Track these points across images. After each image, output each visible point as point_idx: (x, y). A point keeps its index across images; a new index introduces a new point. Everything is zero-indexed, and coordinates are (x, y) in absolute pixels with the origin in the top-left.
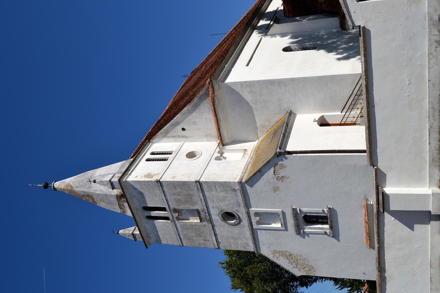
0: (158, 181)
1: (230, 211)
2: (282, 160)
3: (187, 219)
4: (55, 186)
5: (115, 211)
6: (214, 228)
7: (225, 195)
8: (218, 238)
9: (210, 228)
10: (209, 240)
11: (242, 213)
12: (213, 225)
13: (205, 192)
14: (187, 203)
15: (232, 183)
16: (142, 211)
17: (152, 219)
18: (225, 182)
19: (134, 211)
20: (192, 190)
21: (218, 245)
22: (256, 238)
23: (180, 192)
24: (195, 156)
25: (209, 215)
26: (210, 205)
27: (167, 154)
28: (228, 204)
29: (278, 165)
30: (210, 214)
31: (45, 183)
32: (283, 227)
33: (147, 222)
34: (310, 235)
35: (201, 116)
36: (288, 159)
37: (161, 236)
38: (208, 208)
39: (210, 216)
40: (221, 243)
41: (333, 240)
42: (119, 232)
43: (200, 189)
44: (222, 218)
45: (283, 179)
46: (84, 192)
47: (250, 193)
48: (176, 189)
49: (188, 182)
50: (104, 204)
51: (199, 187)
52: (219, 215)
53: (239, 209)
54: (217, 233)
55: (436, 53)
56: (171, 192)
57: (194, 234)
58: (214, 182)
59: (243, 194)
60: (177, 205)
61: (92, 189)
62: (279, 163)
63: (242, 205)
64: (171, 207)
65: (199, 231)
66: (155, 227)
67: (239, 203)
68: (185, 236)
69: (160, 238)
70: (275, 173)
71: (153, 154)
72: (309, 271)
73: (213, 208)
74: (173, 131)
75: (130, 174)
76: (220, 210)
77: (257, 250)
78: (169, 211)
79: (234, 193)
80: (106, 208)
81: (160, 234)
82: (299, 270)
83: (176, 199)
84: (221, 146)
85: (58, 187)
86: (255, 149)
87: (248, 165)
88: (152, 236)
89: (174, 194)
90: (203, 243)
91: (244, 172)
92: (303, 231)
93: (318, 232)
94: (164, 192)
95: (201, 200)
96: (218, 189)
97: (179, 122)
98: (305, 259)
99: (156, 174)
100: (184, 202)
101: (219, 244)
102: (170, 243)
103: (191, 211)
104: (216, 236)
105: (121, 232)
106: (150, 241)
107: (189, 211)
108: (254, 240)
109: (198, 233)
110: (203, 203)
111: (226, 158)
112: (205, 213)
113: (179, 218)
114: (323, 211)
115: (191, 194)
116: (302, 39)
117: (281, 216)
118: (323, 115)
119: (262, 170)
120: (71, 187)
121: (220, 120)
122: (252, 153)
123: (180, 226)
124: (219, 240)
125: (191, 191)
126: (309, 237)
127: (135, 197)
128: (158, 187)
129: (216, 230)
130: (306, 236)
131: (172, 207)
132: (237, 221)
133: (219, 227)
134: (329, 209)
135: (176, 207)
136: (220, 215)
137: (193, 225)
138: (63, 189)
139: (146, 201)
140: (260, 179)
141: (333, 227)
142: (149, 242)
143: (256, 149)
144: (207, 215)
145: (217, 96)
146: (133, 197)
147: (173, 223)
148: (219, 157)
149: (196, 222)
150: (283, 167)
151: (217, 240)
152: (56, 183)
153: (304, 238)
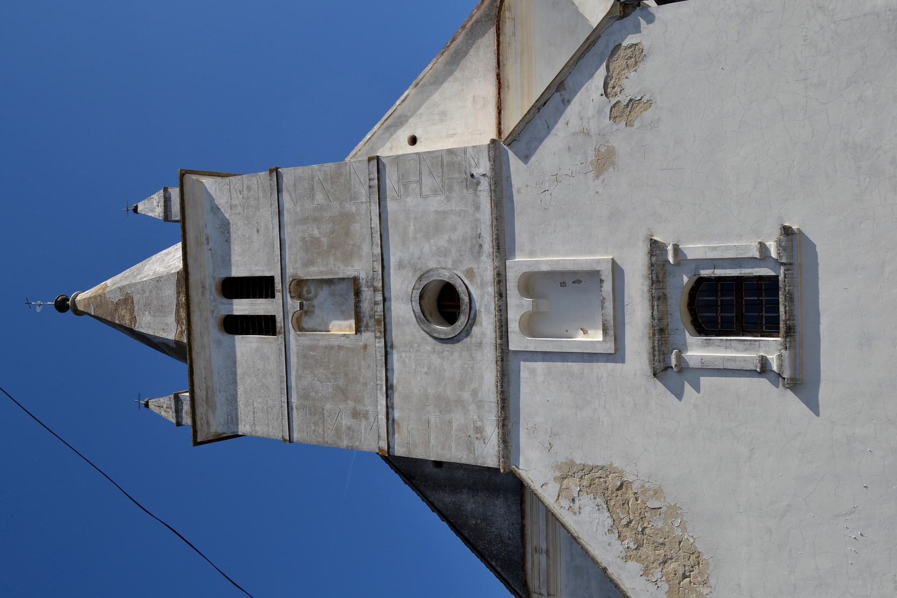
2: (637, 29)
9: (378, 356)
11: (483, 285)
12: (389, 345)
21: (390, 439)
22: (512, 401)
25: (384, 300)
29: (621, 52)
30: (386, 295)
32: (608, 338)
34: (705, 381)
35: (463, 90)
36: (656, 21)
41: (793, 403)
45: (630, 112)
47: (519, 191)
53: (474, 266)
62: (625, 44)
63: (488, 246)
68: (305, 396)
70: (609, 90)
72: (684, 576)
74: (386, 146)
77: (507, 458)
82: (646, 572)
92: (679, 358)
93: (734, 359)
95: (372, 234)
97: (405, 116)
98: (674, 511)
106: (211, 420)
108: (503, 408)
114: (763, 247)
117: (607, 286)
119: (569, 83)
121: (506, 58)
126: (698, 391)
130: (688, 387)
134: (787, 231)
140: (556, 122)
141: (798, 329)
144: (379, 298)
145: (512, 9)
150: (637, 55)
151: (390, 410)
153: (679, 394)
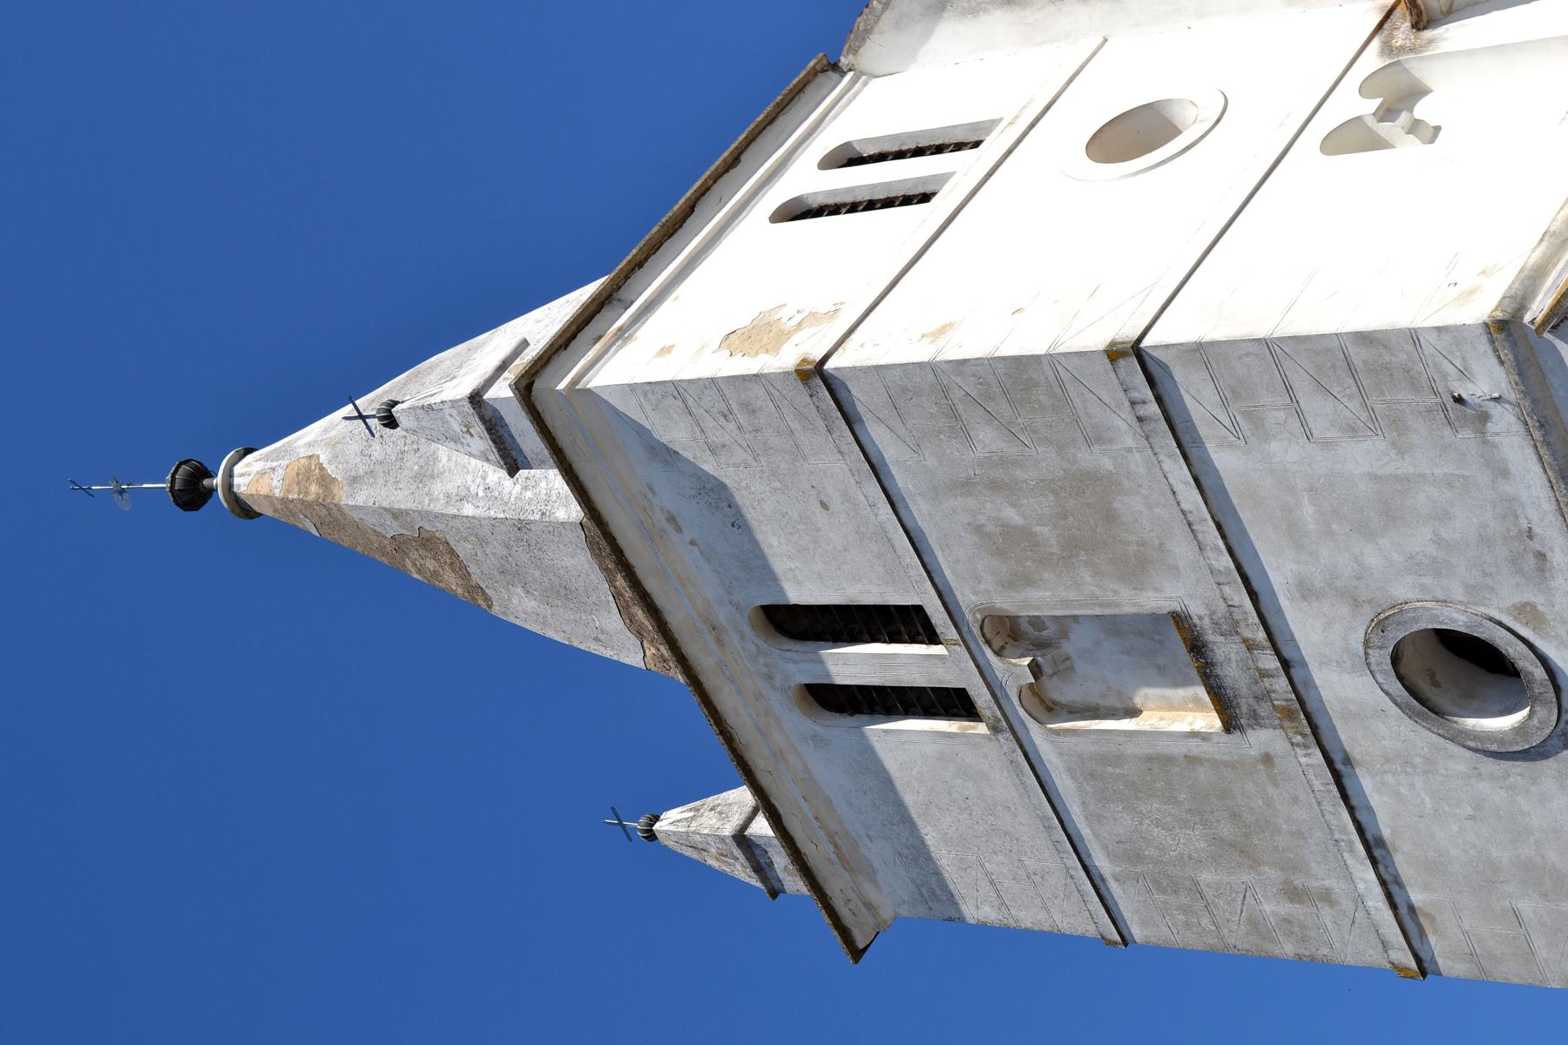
0: (815, 374)
1: (1457, 620)
3: (1118, 705)
4: (239, 486)
5: (608, 653)
6: (1347, 782)
7: (1388, 470)
8: (1404, 878)
10: (1327, 897)
13: (1210, 446)
14: (1083, 556)
15: (1432, 338)
16: (759, 650)
17: (852, 715)
18: (1365, 339)
19: (691, 649)
20: (1099, 440)
21: (1416, 943)
23: (1003, 461)
24: (1172, 131)
25: (1286, 665)
26: (1279, 572)
27: (939, 149)
28: (1432, 550)
30: (1288, 653)
31: (181, 463)
33: (814, 737)
37: (944, 858)
38: (1263, 598)
39: (1293, 671)
40: (1432, 919)
42: (657, 827)
43: (1164, 426)
44: (1397, 688)
46: (396, 514)
48: (965, 435)
49: (1051, 360)
50: (533, 603)
51: (1144, 402)
52: (1372, 660)
53: (1538, 600)
54: (1386, 833)
56: (931, 462)
57: (1194, 841)
58: (1265, 342)
59: (1547, 444)
60: (1012, 583)
61: (438, 488)
64: (960, 598)
65: (1234, 816)
66: (887, 782)
67: (1530, 534)
68: (1131, 854)
69: (937, 873)
71: (849, 157)
73: (1304, 597)
75: (623, 334)
76: (1368, 613)
78: (956, 636)
79: (1466, 434)
80: (551, 634)
81: (931, 837)
83: (990, 528)
84: (1402, 31)
85: (254, 492)
88: (876, 852)
89: (966, 486)
90: (1287, 921)
94: (877, 470)
95: (1190, 525)
96: (1317, 408)
99: (814, 318)
100: (1055, 550)
101: (1422, 933)
102: (1028, 917)
103: (1141, 634)
104: (1377, 853)
105: (671, 822)
107: (1113, 626)
109: (1226, 830)
110: (1210, 553)
111: (1437, 129)
112: (1250, 646)
113: (1054, 703)
115: (1092, 478)
120: (326, 481)
123: (1069, 770)
124: (1417, 897)
125: (1096, 448)
127: (679, 530)
128: (820, 423)
129: (1375, 800)
131: (966, 598)
132: (1541, 712)
133: (1389, 778)
135: (1006, 603)
136: (1382, 658)
137: (1168, 760)
138: (285, 501)
139: (761, 556)
142: (868, 905)
144: (1270, 662)
146: (667, 526)
147: (1006, 739)
148: (1372, 123)
149: (1194, 734)
151: (1394, 888)
152: (249, 458)
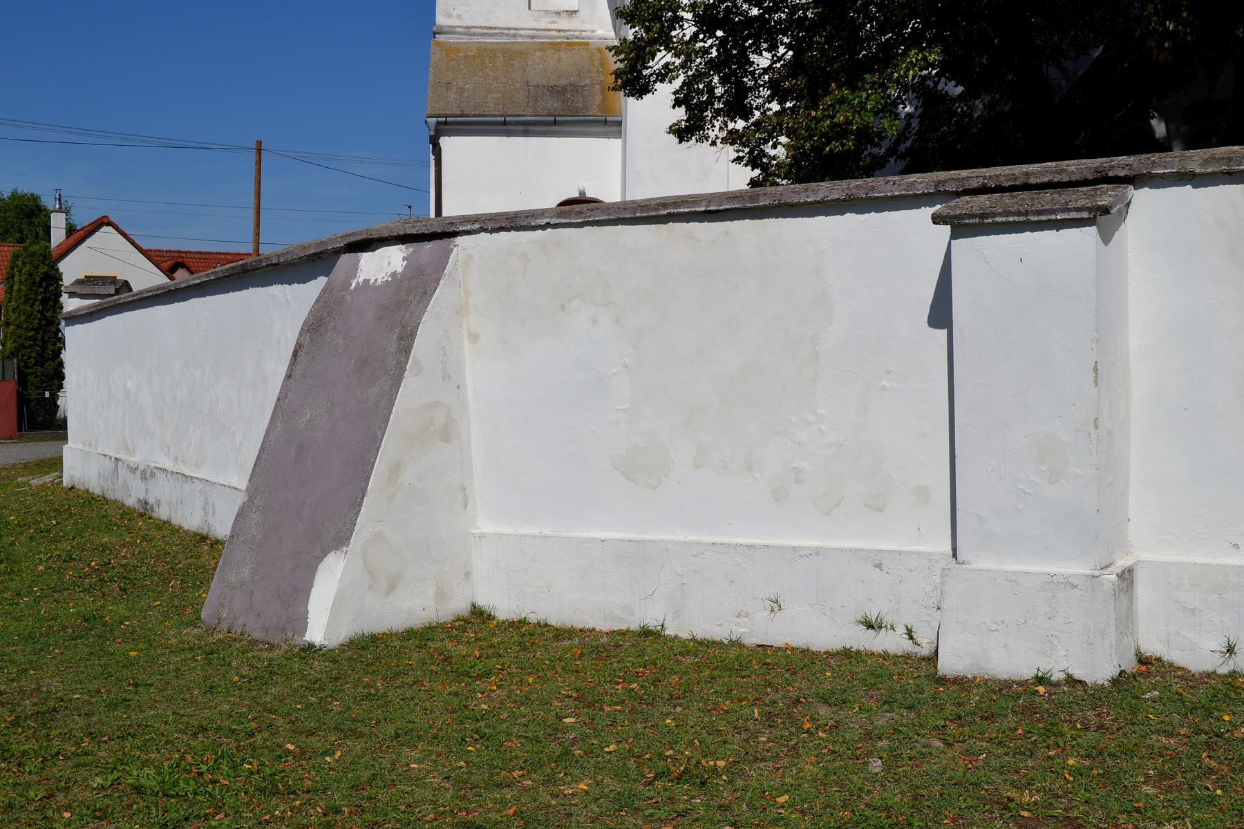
55: (445, 806)
86: (577, 37)
87: (503, 33)
91: (472, 30)
116: (354, 285)
118: (67, 439)
122: (557, 33)
143: (578, 40)
